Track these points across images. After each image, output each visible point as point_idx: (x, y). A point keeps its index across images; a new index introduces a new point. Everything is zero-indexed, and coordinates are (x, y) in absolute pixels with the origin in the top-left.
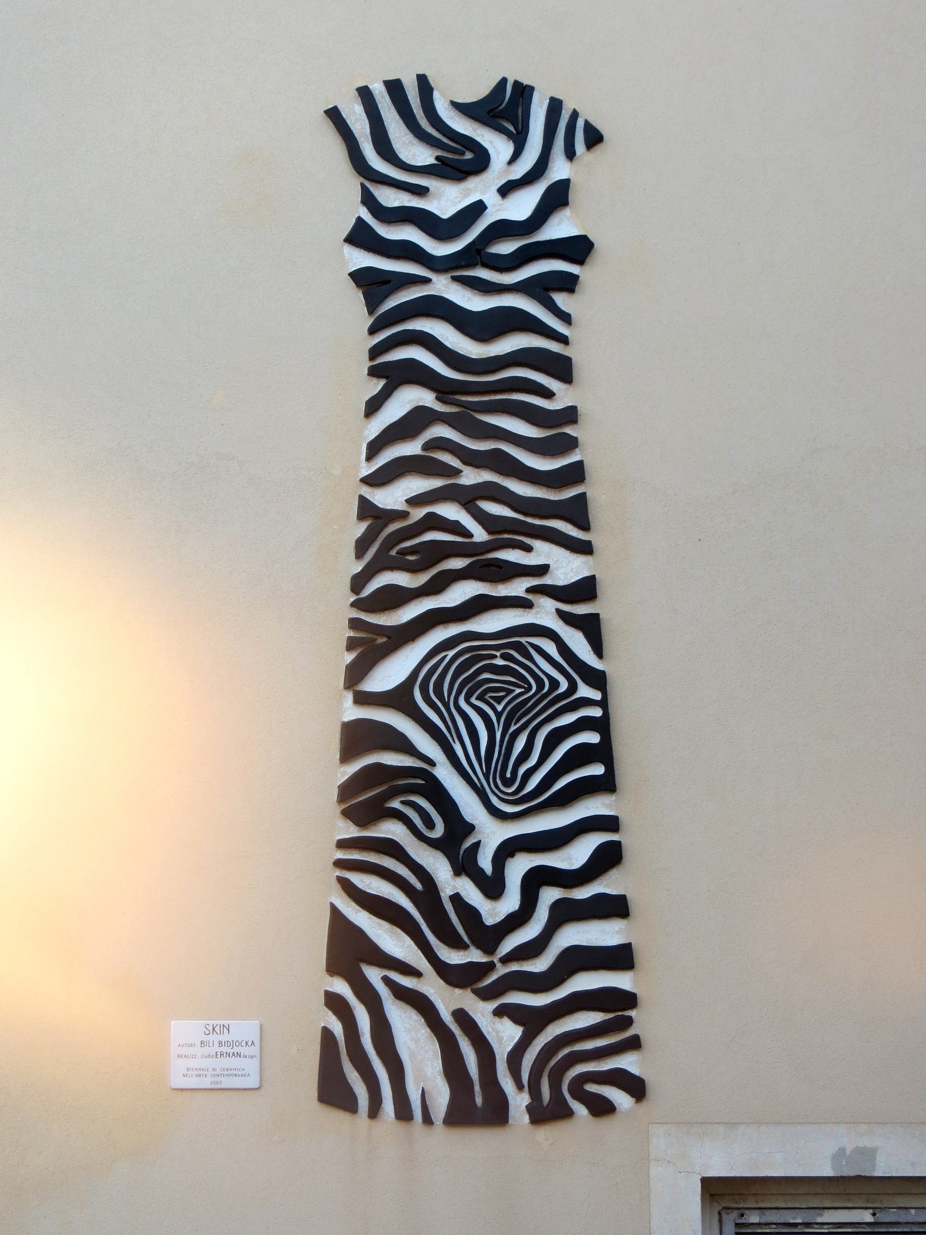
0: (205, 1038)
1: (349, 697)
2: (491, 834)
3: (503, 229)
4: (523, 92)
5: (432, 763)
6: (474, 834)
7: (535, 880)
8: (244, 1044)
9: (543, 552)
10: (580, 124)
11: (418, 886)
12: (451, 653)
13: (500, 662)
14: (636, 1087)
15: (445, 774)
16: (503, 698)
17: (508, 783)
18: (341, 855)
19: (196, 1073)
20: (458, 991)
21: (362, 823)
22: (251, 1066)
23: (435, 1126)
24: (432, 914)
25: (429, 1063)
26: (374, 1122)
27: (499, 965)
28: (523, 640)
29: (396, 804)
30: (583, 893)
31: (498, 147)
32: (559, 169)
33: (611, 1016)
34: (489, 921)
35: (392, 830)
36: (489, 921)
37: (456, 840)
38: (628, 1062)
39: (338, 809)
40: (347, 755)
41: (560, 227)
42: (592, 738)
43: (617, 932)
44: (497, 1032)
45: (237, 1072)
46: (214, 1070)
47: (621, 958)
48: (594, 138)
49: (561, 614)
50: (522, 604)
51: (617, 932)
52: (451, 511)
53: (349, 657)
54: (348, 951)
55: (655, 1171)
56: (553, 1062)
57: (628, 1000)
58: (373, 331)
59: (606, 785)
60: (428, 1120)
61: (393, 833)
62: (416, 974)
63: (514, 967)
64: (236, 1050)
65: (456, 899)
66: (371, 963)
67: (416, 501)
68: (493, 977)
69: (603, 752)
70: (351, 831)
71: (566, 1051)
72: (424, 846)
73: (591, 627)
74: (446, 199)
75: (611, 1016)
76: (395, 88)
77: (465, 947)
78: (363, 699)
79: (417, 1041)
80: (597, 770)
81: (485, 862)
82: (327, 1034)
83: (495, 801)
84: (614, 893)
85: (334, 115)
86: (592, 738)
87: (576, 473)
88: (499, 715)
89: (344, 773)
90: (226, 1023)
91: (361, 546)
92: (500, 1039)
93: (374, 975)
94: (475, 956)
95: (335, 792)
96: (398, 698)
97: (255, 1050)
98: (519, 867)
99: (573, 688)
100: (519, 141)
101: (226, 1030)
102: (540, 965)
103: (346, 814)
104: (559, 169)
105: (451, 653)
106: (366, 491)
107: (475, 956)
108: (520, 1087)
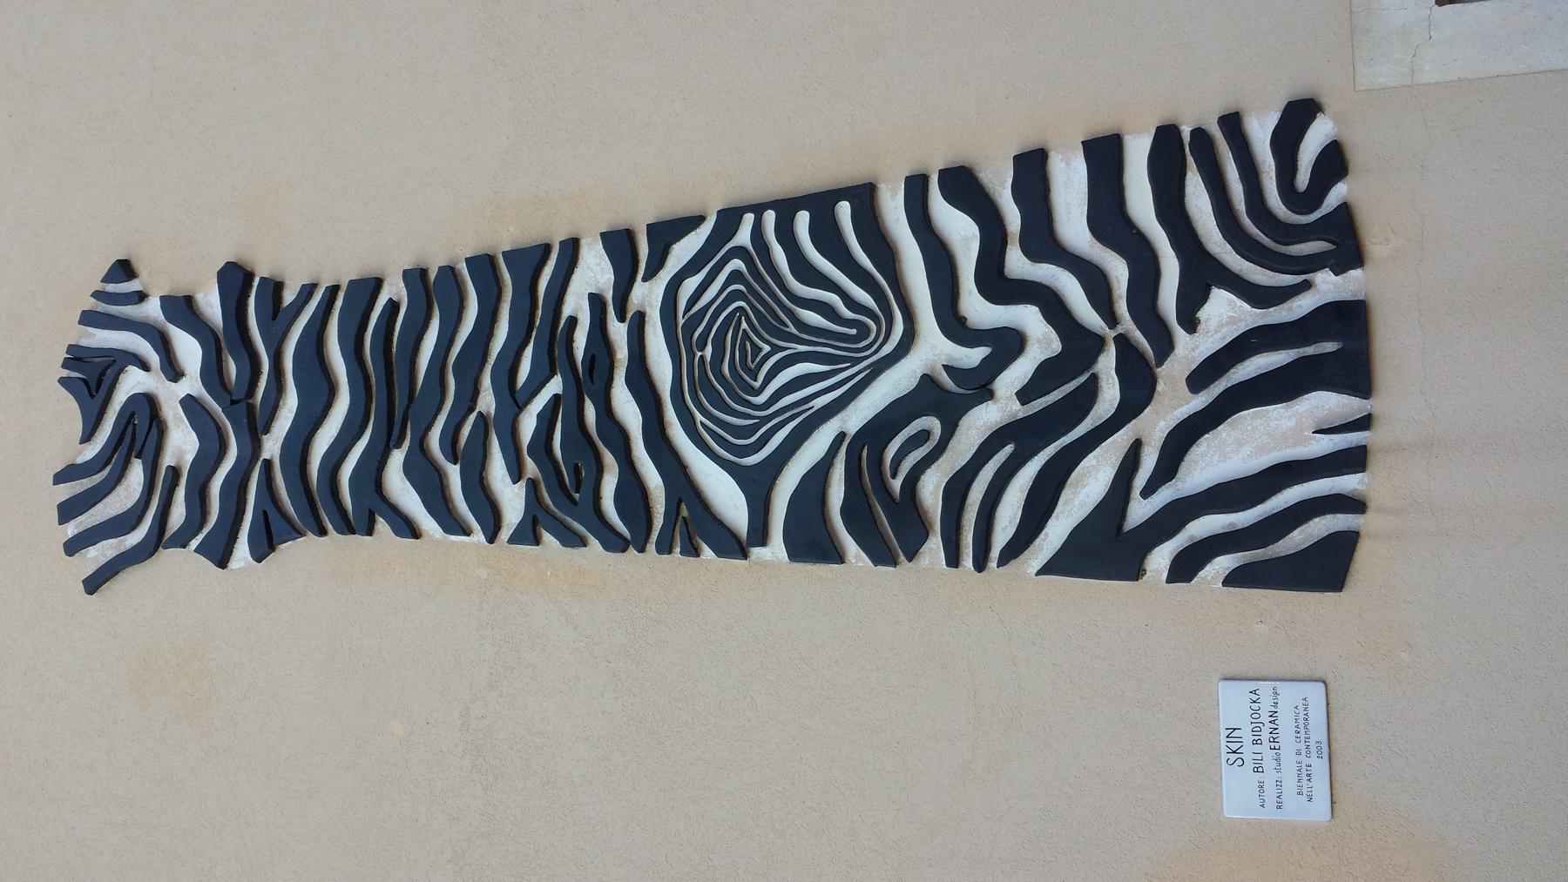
0: (1249, 765)
1: (757, 552)
2: (934, 350)
3: (212, 373)
4: (77, 357)
5: (841, 436)
6: (935, 375)
7: (996, 285)
8: (1255, 706)
9: (576, 303)
10: (111, 288)
11: (1009, 449)
12: (699, 417)
13: (709, 350)
14: (1299, 114)
15: (855, 418)
16: (752, 343)
17: (864, 331)
18: (968, 561)
19: (1305, 782)
20: (1160, 387)
21: (924, 534)
22: (1291, 695)
23: (1375, 412)
24: (1051, 428)
25: (1273, 424)
26: (1372, 505)
27: (1120, 329)
28: (681, 321)
29: (897, 484)
30: (1013, 218)
31: (133, 382)
32: (152, 309)
33: (1190, 160)
34: (1056, 346)
35: (932, 489)
36: (1056, 346)
37: (944, 399)
38: (1260, 131)
39: (904, 563)
40: (834, 555)
41: (211, 304)
42: (803, 220)
43: (1068, 164)
44: (1221, 325)
45: (1301, 716)
46: (1299, 753)
47: (1104, 155)
48: (124, 269)
49: (650, 275)
50: (638, 326)
51: (1068, 164)
52: (528, 425)
53: (707, 552)
54: (1107, 549)
55: (1430, 73)
56: (1266, 240)
57: (1166, 138)
58: (322, 532)
59: (864, 197)
60: (1364, 423)
61: (936, 487)
62: (1136, 448)
63: (1122, 308)
64: (1265, 718)
65: (1025, 395)
66: (1123, 515)
67: (516, 473)
68: (1138, 337)
69: (821, 204)
70: (934, 546)
71: (1247, 222)
72: (953, 443)
73: (666, 232)
74: (182, 444)
75: (1190, 160)
76: (67, 511)
77: (1094, 379)
78: (759, 534)
79: (1240, 443)
80: (844, 210)
81: (973, 356)
82: (1234, 579)
83: (888, 349)
84: (1011, 173)
85: (93, 584)
86: (803, 220)
87: (484, 266)
88: (776, 349)
89: (856, 557)
90: (1224, 733)
91: (572, 540)
92: (1232, 321)
93: (1140, 510)
94: (1107, 364)
95: (882, 569)
96: (757, 486)
97: (1265, 688)
98: (978, 310)
99: (740, 252)
100: (121, 360)
101: (1236, 734)
102: (1118, 271)
103: (911, 555)
104: (152, 309)
105: (699, 417)
106: (505, 534)
107: (1107, 364)
108: (1306, 286)
